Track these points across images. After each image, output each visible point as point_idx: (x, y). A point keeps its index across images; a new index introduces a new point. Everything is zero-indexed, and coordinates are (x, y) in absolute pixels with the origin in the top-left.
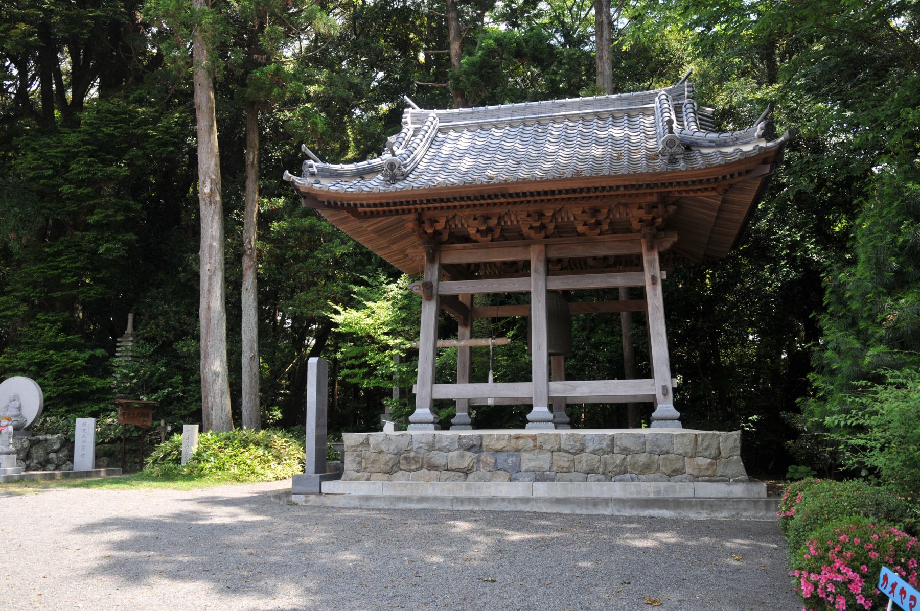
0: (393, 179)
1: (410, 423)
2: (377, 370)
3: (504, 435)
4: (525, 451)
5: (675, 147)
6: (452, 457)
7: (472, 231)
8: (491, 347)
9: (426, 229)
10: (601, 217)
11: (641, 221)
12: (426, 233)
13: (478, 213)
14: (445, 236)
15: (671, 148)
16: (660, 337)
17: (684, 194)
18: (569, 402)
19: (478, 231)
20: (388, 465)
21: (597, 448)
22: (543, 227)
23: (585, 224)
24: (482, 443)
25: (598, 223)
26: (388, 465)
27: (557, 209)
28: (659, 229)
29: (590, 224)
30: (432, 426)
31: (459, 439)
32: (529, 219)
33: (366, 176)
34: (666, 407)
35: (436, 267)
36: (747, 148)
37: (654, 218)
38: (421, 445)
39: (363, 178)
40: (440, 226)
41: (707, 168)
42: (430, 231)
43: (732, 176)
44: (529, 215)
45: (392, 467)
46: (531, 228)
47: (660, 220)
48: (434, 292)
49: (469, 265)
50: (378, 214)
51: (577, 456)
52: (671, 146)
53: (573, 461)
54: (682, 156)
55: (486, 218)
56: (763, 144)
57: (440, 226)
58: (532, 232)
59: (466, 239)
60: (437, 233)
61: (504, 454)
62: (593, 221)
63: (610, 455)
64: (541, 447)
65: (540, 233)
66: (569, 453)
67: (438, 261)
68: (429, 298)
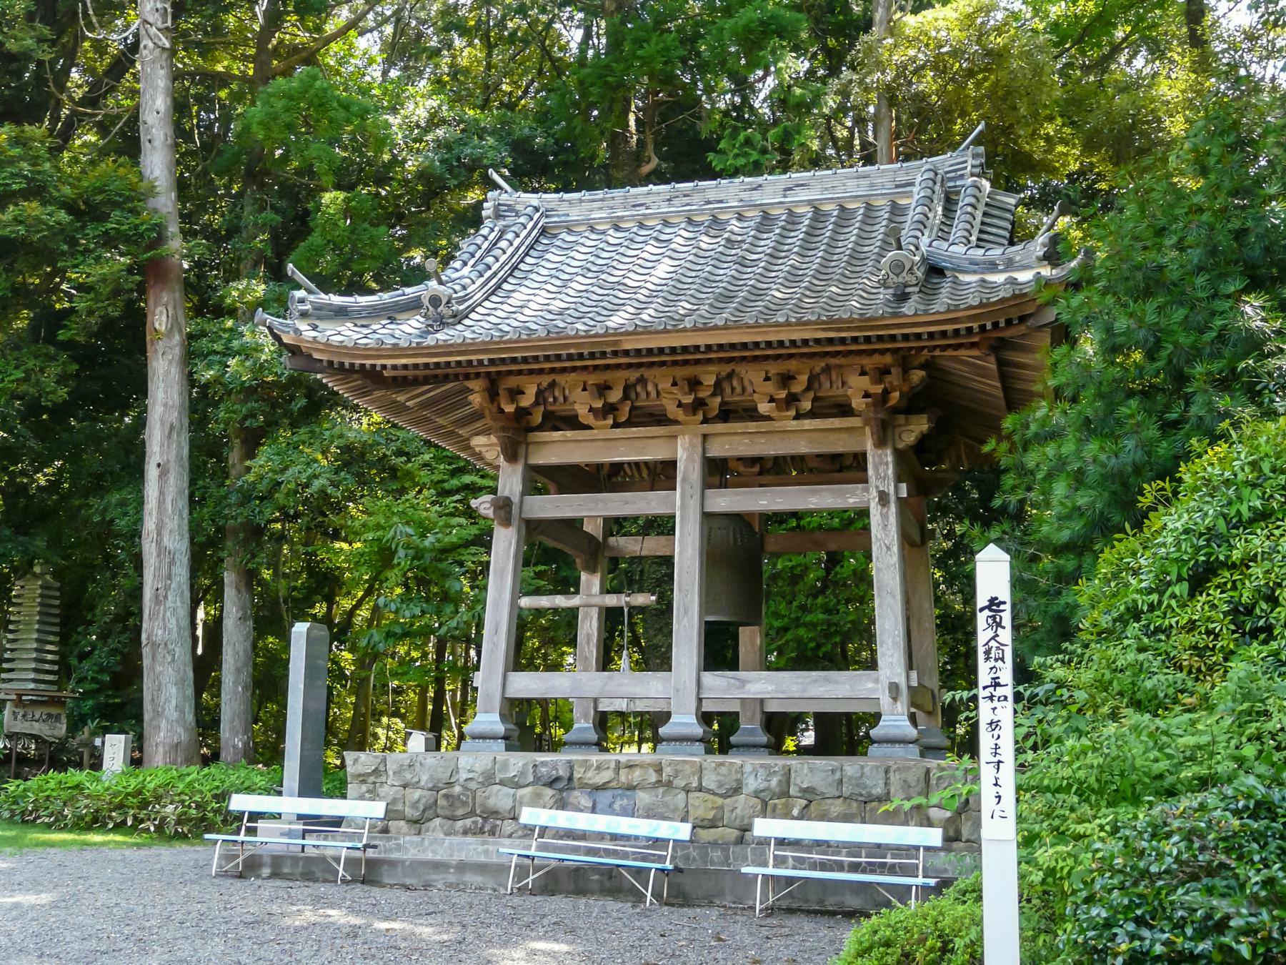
0: (442, 322)
1: (873, 742)
2: (861, 640)
3: (610, 761)
4: (643, 788)
5: (904, 274)
6: (521, 797)
7: (582, 411)
8: (626, 610)
9: (503, 406)
10: (797, 388)
11: (867, 395)
12: (502, 411)
13: (592, 379)
14: (537, 418)
15: (897, 275)
16: (890, 599)
17: (937, 353)
18: (772, 707)
19: (591, 410)
20: (417, 808)
21: (762, 786)
22: (699, 404)
23: (772, 400)
24: (572, 774)
25: (792, 399)
26: (417, 808)
27: (724, 374)
28: (895, 411)
29: (687, 404)
30: (699, 747)
31: (535, 766)
32: (675, 390)
33: (399, 316)
34: (895, 720)
35: (519, 468)
36: (1024, 276)
37: (886, 392)
38: (471, 775)
39: (392, 320)
40: (527, 401)
41: (981, 305)
42: (509, 409)
43: (1009, 322)
44: (675, 384)
45: (424, 811)
46: (680, 405)
47: (896, 395)
48: (515, 510)
49: (599, 466)
50: (426, 380)
51: (728, 800)
52: (897, 271)
53: (721, 808)
54: (917, 289)
55: (603, 389)
56: (1046, 271)
57: (527, 401)
58: (680, 411)
59: (573, 423)
60: (522, 413)
61: (609, 794)
62: (782, 394)
63: (783, 800)
64: (669, 784)
65: (694, 414)
66: (715, 794)
67: (522, 461)
68: (507, 522)
